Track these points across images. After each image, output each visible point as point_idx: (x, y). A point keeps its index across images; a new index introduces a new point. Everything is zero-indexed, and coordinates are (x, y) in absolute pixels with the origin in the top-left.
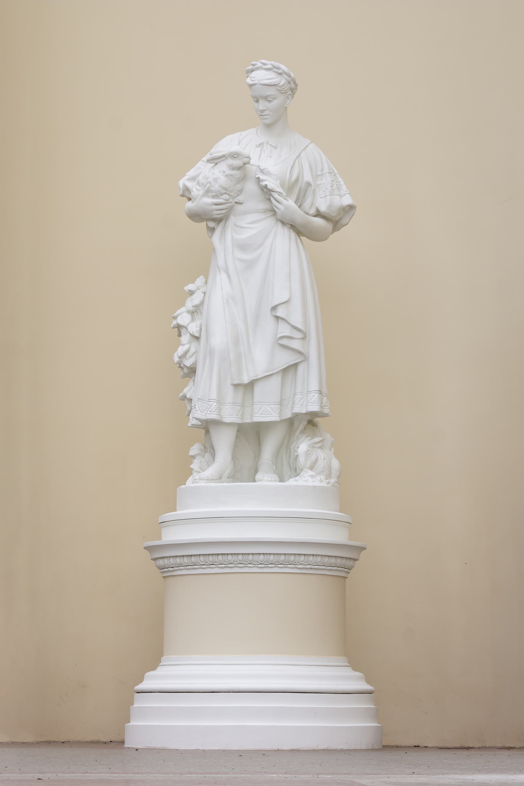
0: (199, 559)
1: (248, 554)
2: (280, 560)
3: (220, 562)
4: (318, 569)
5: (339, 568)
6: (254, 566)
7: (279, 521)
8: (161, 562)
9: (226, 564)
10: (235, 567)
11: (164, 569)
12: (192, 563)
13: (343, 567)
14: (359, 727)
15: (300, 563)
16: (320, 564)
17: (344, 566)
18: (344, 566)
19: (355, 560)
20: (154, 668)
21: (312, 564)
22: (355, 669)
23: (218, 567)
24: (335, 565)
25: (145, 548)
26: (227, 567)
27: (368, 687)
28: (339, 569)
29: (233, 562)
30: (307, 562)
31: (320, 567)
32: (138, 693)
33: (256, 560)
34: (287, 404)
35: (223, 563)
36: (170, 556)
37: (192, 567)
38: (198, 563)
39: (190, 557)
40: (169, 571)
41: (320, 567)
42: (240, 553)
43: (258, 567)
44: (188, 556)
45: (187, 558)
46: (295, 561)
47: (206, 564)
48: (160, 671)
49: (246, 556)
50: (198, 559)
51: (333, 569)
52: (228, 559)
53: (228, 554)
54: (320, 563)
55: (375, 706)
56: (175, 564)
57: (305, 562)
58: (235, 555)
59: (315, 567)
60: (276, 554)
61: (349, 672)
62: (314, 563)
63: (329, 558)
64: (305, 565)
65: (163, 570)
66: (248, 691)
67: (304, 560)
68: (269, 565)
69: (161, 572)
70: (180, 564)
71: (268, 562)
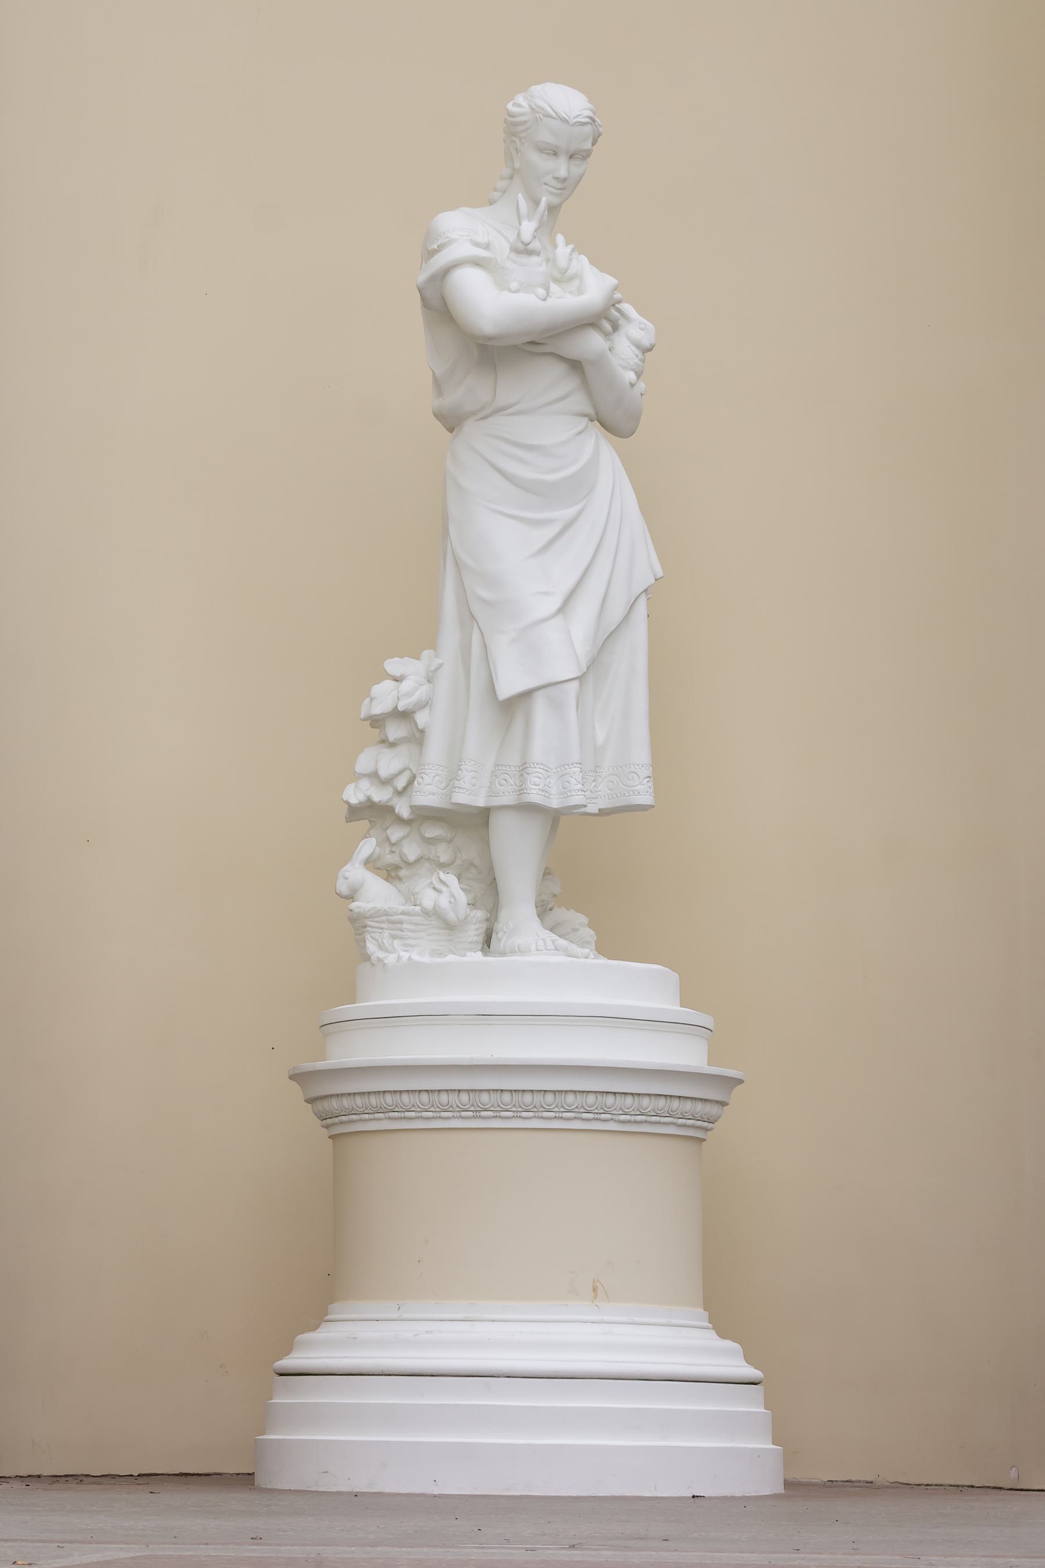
0: (419, 1099)
1: (523, 1091)
2: (605, 1105)
3: (423, 1107)
4: (636, 1122)
5: (699, 1122)
6: (514, 1116)
7: (599, 1024)
8: (325, 1105)
9: (476, 1111)
10: (594, 1119)
11: (339, 1118)
12: (438, 1104)
13: (700, 1119)
14: (754, 1450)
15: (669, 1114)
16: (664, 1112)
17: (702, 1118)
18: (702, 1118)
19: (723, 1104)
20: (314, 1328)
21: (675, 1116)
22: (722, 1334)
23: (498, 1116)
24: (668, 1112)
25: (292, 1077)
26: (597, 1119)
27: (752, 1372)
28: (699, 1123)
29: (490, 1107)
30: (602, 1108)
31: (663, 1120)
32: (281, 1375)
33: (538, 1105)
34: (601, 780)
35: (410, 1108)
36: (331, 1093)
37: (372, 1116)
38: (416, 1106)
39: (417, 1093)
40: (350, 1122)
41: (663, 1120)
42: (505, 1089)
43: (542, 1117)
44: (395, 1092)
45: (347, 1099)
46: (615, 1107)
47: (396, 1110)
48: (324, 1333)
49: (497, 1094)
50: (436, 1097)
51: (662, 1121)
52: (459, 1101)
53: (401, 1092)
54: (631, 1109)
55: (765, 1409)
56: (379, 1106)
57: (597, 1108)
58: (496, 1092)
59: (639, 1118)
60: (579, 1091)
61: (711, 1338)
62: (635, 1110)
63: (650, 1099)
64: (663, 1116)
65: (329, 1121)
66: (607, 1377)
67: (633, 1105)
68: (564, 1113)
69: (323, 1126)
70: (349, 1109)
71: (563, 1107)
